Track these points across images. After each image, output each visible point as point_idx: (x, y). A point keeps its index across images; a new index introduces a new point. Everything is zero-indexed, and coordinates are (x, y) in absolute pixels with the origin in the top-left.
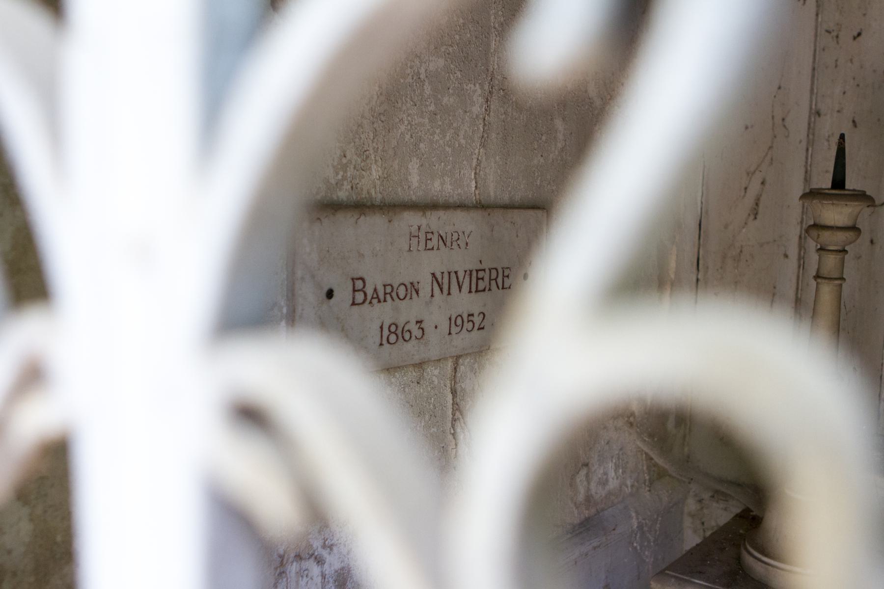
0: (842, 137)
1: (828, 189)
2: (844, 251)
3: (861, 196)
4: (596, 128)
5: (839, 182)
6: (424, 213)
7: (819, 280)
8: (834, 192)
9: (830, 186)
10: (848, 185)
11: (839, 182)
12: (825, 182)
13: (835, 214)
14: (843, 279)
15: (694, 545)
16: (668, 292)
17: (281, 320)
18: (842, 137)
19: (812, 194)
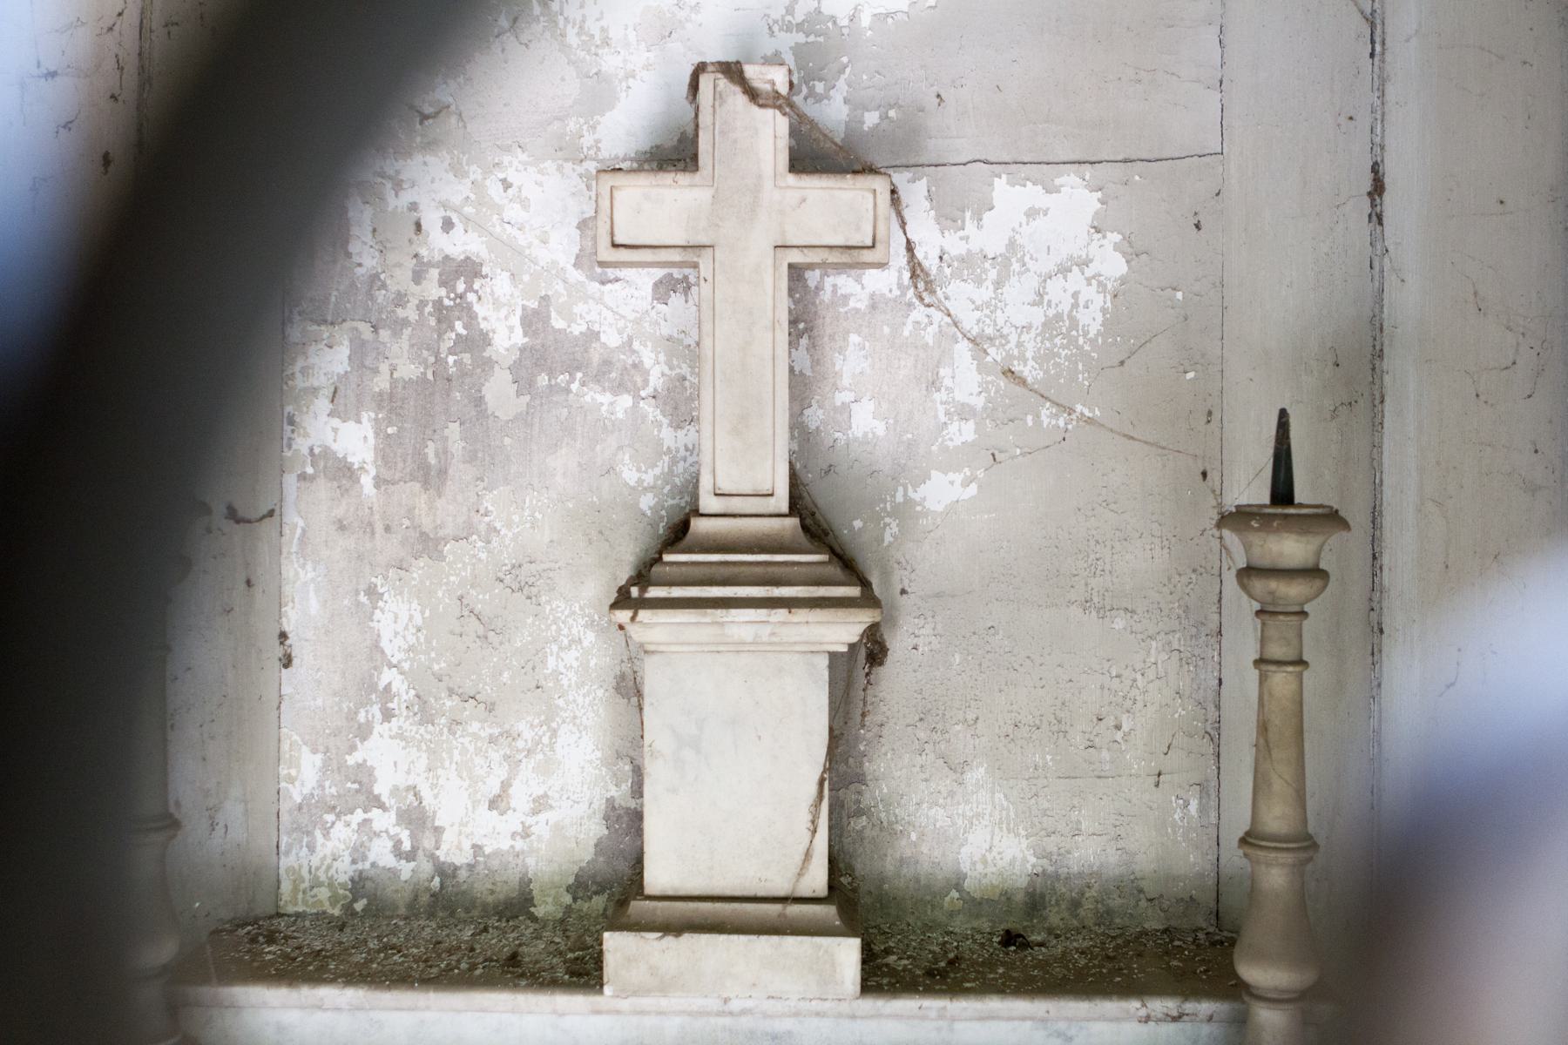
0: (1283, 414)
1: (1265, 506)
2: (1304, 614)
3: (1331, 519)
4: (481, 888)
5: (1282, 492)
6: (345, 457)
7: (1264, 667)
8: (1279, 510)
9: (1267, 501)
10: (1299, 497)
11: (1282, 492)
12: (1260, 494)
13: (1290, 548)
14: (1301, 662)
15: (826, 674)
16: (1019, 897)
17: (991, 185)
18: (1283, 414)
19: (1239, 518)
